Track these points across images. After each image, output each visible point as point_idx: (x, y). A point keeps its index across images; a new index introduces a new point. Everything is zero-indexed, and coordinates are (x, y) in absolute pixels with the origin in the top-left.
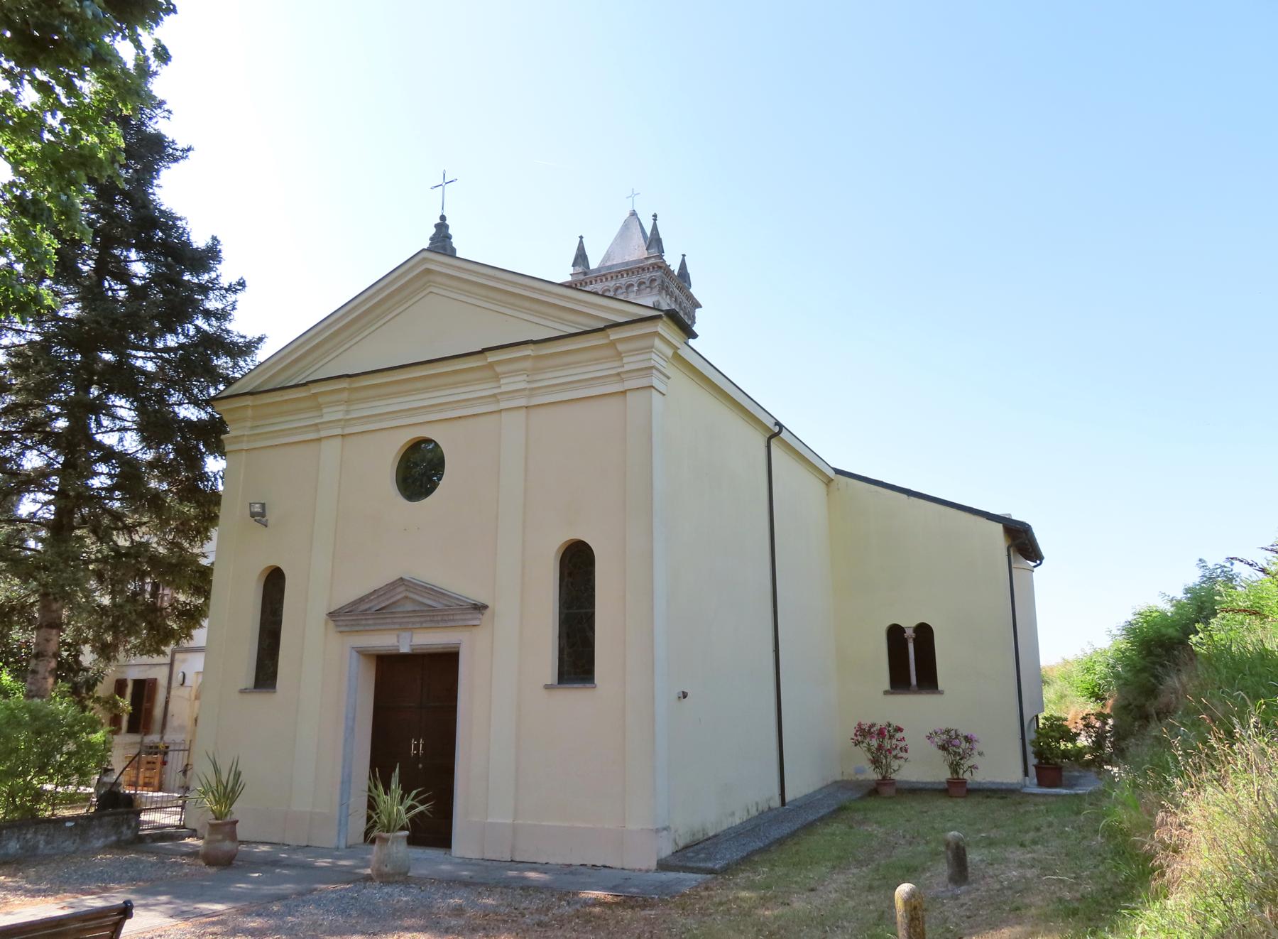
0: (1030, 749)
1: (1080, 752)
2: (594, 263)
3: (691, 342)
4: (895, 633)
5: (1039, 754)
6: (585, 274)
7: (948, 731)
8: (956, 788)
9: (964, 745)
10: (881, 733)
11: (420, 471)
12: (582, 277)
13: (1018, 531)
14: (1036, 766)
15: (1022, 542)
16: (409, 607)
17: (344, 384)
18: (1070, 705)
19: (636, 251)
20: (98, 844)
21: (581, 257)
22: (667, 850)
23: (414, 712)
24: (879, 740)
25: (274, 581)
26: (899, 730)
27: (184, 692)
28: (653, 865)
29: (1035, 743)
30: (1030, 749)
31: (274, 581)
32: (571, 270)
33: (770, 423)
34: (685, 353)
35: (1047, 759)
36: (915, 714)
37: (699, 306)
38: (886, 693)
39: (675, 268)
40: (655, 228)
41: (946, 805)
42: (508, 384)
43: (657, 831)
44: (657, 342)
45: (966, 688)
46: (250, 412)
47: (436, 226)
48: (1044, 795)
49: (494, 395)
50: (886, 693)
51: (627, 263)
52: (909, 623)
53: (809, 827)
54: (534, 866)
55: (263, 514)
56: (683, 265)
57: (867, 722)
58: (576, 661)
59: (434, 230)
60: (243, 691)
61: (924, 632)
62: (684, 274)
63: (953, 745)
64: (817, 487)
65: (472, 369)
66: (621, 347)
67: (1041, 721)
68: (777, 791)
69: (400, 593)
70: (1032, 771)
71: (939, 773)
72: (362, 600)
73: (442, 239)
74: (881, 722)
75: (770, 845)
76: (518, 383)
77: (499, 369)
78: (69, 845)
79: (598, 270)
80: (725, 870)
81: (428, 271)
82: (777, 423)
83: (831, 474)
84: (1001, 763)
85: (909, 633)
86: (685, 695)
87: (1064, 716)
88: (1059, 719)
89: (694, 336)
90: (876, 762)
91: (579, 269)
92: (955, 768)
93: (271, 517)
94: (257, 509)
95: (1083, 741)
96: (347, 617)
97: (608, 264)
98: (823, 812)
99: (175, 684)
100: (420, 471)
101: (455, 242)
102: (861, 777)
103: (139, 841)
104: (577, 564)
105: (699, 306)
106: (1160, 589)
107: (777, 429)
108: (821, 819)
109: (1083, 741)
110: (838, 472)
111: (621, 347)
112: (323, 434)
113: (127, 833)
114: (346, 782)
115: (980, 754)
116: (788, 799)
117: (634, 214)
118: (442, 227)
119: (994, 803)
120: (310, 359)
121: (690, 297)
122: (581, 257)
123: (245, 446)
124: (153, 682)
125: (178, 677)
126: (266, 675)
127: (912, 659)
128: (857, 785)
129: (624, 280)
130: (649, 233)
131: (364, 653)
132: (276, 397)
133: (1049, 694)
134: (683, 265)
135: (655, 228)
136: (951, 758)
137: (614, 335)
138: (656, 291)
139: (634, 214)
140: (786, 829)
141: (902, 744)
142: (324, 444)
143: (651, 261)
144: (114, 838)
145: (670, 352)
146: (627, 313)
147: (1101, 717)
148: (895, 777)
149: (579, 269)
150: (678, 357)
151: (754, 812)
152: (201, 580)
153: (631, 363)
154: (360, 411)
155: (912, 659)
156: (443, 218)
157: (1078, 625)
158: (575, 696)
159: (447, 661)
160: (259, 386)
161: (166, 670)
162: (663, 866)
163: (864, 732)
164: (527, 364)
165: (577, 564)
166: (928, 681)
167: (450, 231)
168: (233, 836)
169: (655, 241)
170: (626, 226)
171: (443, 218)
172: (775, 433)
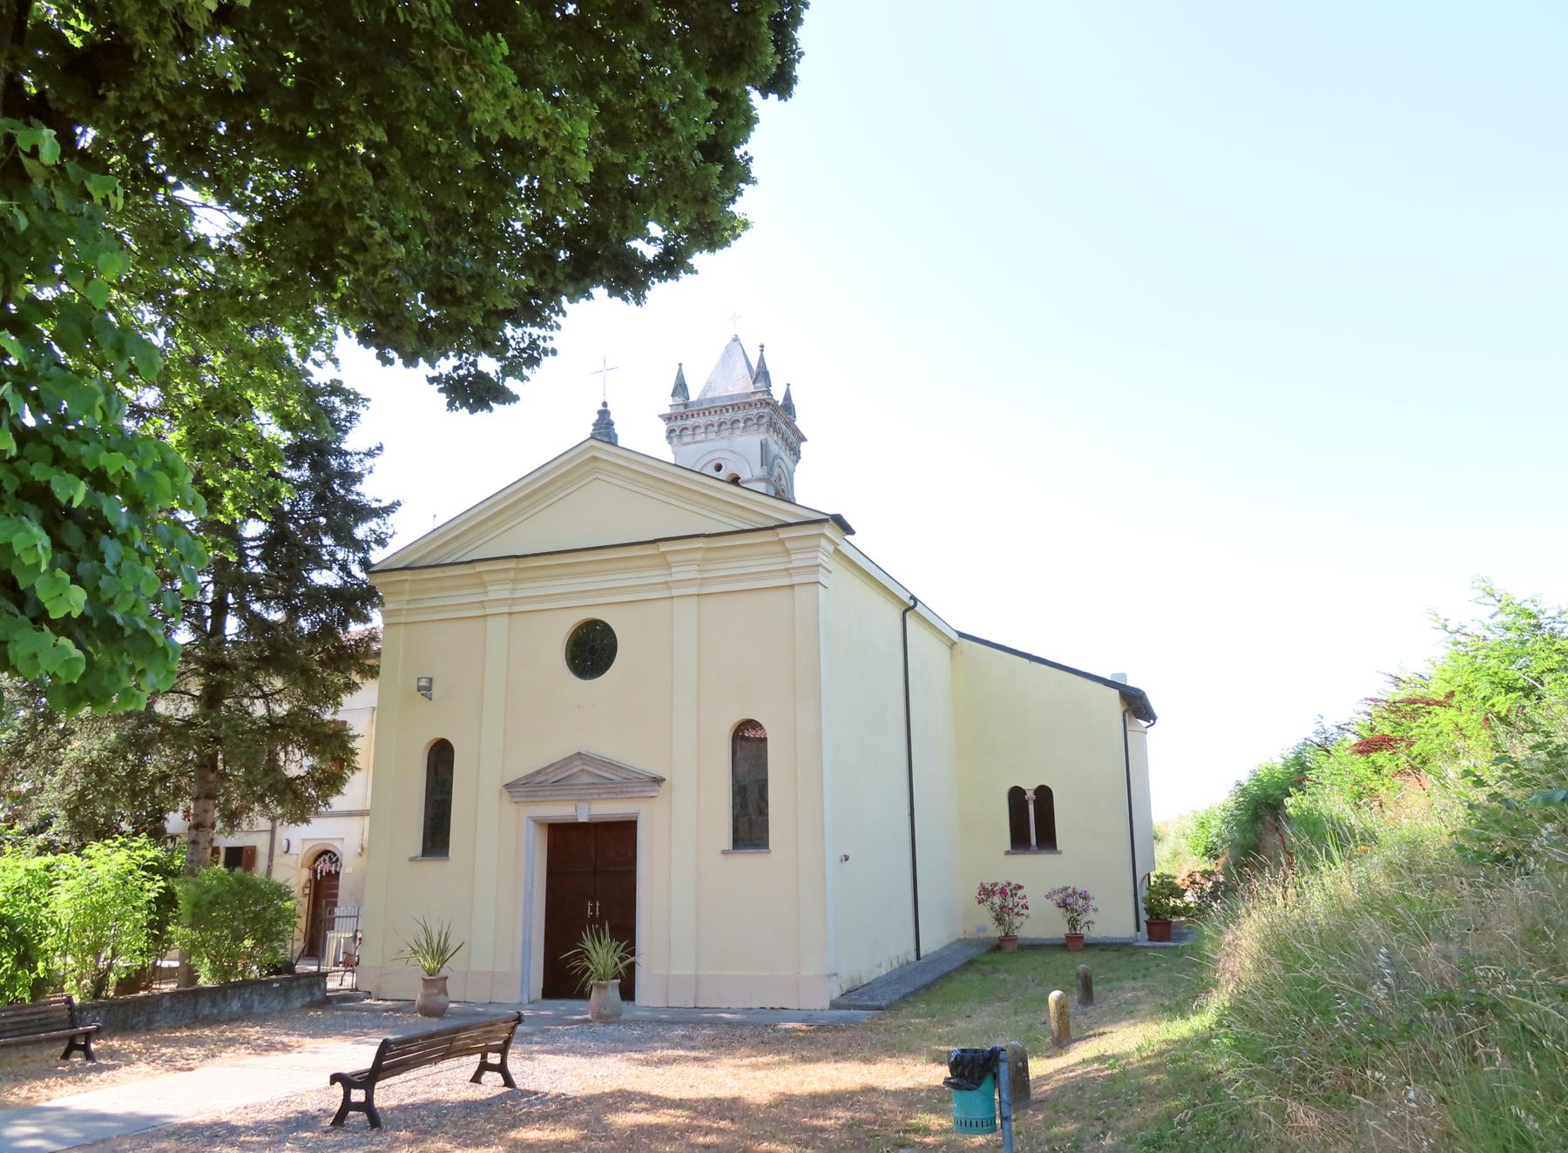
0: (1142, 906)
1: (1187, 908)
2: (694, 395)
3: (848, 537)
4: (1016, 795)
5: (1150, 911)
6: (686, 406)
7: (1066, 889)
8: (1074, 943)
9: (1081, 902)
10: (1003, 892)
11: (591, 650)
12: (682, 409)
13: (1134, 697)
14: (1148, 923)
15: (1136, 705)
16: (586, 779)
17: (512, 564)
18: (1180, 856)
19: (739, 384)
20: (297, 1003)
21: (680, 387)
22: (836, 994)
23: (590, 878)
24: (1001, 899)
25: (441, 756)
26: (1020, 887)
27: (287, 859)
28: (827, 1005)
29: (1148, 900)
30: (1142, 906)
31: (441, 756)
32: (670, 401)
33: (906, 598)
34: (844, 548)
35: (1158, 915)
36: (1036, 874)
37: (804, 439)
38: (1007, 853)
39: (779, 397)
40: (762, 360)
41: (1065, 957)
42: (679, 573)
43: (829, 976)
44: (823, 542)
45: (1084, 852)
46: (407, 586)
47: (600, 412)
48: (1154, 947)
49: (666, 583)
50: (1007, 853)
51: (731, 397)
52: (1029, 786)
53: (947, 977)
54: (728, 1010)
55: (429, 688)
56: (788, 397)
57: (988, 881)
58: (749, 826)
59: (596, 417)
60: (412, 860)
61: (1044, 794)
62: (788, 406)
63: (1070, 902)
64: (943, 650)
65: (462, 576)
66: (789, 545)
67: (1153, 879)
68: (912, 946)
69: (577, 767)
70: (1144, 926)
71: (1060, 930)
72: (538, 773)
73: (604, 428)
74: (1002, 882)
75: (918, 990)
76: (690, 572)
77: (670, 558)
78: (276, 1005)
79: (700, 402)
80: (889, 1007)
81: (594, 458)
82: (912, 597)
83: (955, 637)
84: (1114, 918)
85: (1030, 795)
86: (847, 858)
87: (1173, 873)
88: (1169, 877)
89: (852, 532)
90: (999, 919)
91: (679, 400)
92: (1073, 923)
93: (435, 692)
94: (423, 683)
95: (1189, 897)
96: (523, 788)
97: (709, 396)
98: (956, 964)
99: (277, 852)
100: (591, 650)
101: (617, 429)
102: (982, 935)
103: (329, 1002)
104: (748, 742)
105: (804, 439)
106: (1266, 753)
107: (912, 603)
108: (956, 970)
109: (1189, 897)
110: (961, 635)
111: (789, 545)
112: (489, 611)
113: (318, 995)
114: (527, 943)
115: (1095, 910)
116: (922, 953)
117: (736, 339)
118: (604, 414)
119: (1109, 955)
120: (469, 536)
121: (796, 432)
122: (680, 387)
123: (402, 619)
124: (253, 850)
125: (280, 845)
126: (436, 838)
127: (1032, 819)
128: (981, 943)
129: (729, 416)
130: (755, 367)
131: (538, 822)
132: (437, 573)
133: (1162, 853)
134: (788, 397)
135: (762, 360)
136: (1069, 915)
137: (783, 534)
138: (763, 428)
139: (736, 339)
140: (927, 978)
141: (1022, 902)
142: (490, 620)
143: (758, 397)
144: (308, 999)
145: (831, 548)
146: (795, 515)
147: (1207, 874)
148: (1016, 933)
149: (679, 400)
150: (837, 551)
151: (896, 965)
152: (334, 747)
153: (798, 560)
154: (527, 589)
155: (1032, 819)
156: (605, 404)
157: (1187, 794)
158: (749, 861)
159: (623, 833)
160: (419, 559)
161: (266, 837)
162: (835, 1005)
163: (986, 892)
164: (699, 555)
165: (748, 742)
166: (1047, 840)
167: (612, 417)
168: (444, 991)
169: (762, 375)
170: (728, 351)
171: (605, 404)
172: (910, 607)
